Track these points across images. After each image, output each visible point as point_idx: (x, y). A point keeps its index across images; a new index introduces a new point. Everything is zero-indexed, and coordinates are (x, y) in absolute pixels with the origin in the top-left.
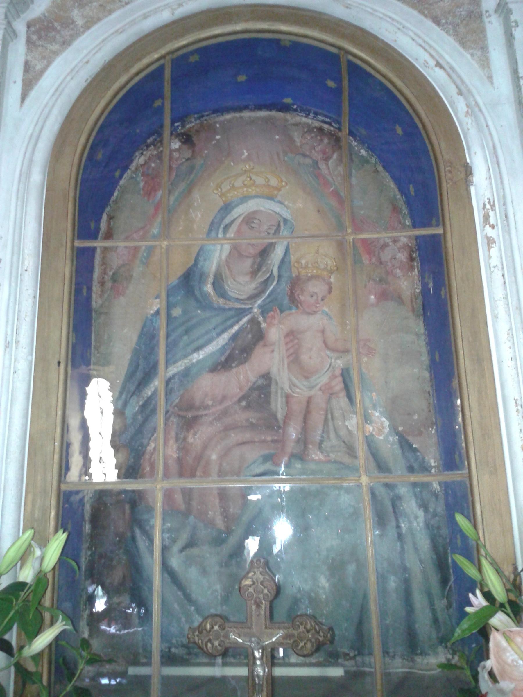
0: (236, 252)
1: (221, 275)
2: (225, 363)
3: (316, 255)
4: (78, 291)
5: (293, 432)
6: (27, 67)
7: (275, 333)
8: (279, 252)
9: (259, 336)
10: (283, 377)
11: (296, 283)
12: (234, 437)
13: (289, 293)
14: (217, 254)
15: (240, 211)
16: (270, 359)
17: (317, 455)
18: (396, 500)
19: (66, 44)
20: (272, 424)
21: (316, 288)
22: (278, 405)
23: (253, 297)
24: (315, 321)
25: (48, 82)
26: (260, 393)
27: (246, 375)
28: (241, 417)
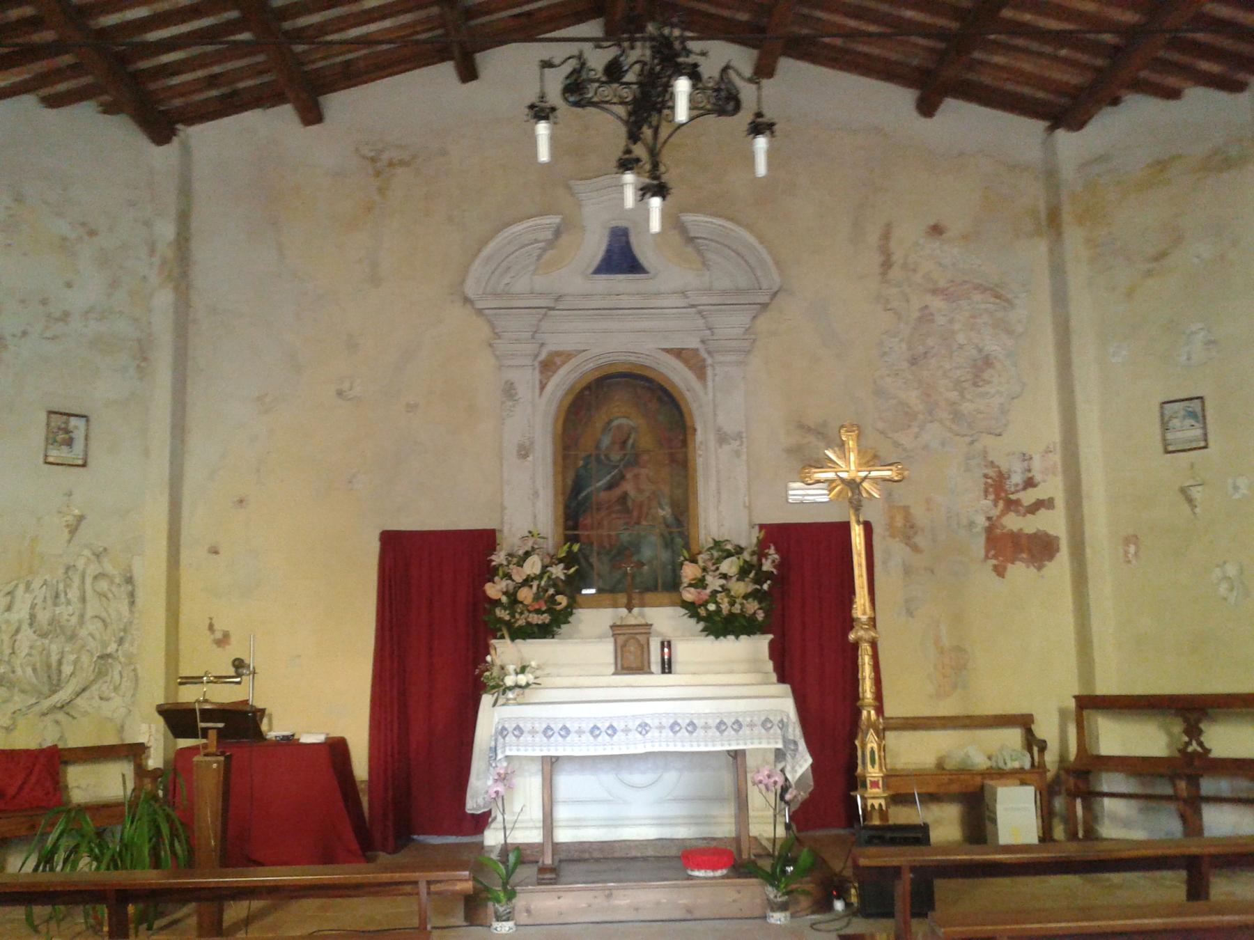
0: (613, 443)
1: (638, 273)
2: (610, 486)
3: (646, 441)
4: (91, 893)
5: (635, 514)
6: (541, 382)
7: (629, 476)
8: (631, 441)
9: (622, 477)
10: (632, 493)
11: (637, 456)
12: (614, 516)
13: (634, 460)
14: (606, 441)
15: (615, 423)
16: (628, 487)
17: (644, 523)
18: (672, 539)
19: (555, 372)
20: (627, 511)
21: (645, 457)
22: (630, 504)
23: (621, 460)
24: (644, 471)
25: (550, 387)
26: (624, 497)
27: (617, 492)
28: (618, 508)
